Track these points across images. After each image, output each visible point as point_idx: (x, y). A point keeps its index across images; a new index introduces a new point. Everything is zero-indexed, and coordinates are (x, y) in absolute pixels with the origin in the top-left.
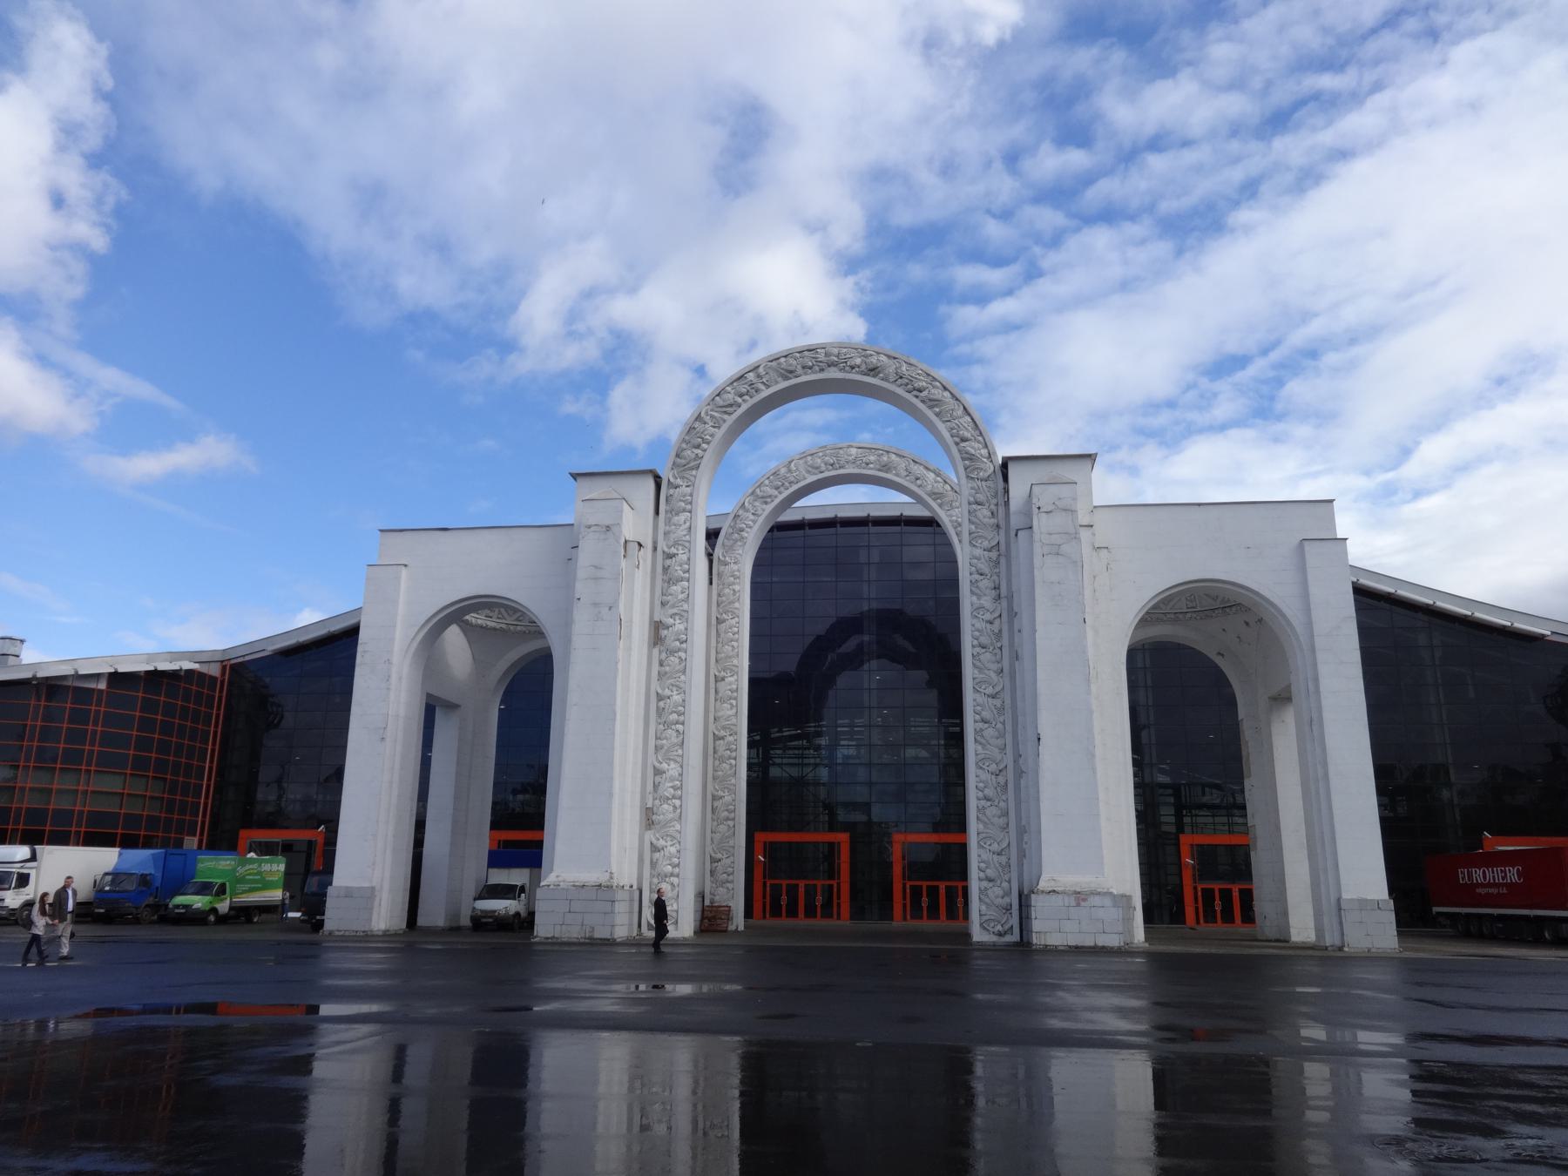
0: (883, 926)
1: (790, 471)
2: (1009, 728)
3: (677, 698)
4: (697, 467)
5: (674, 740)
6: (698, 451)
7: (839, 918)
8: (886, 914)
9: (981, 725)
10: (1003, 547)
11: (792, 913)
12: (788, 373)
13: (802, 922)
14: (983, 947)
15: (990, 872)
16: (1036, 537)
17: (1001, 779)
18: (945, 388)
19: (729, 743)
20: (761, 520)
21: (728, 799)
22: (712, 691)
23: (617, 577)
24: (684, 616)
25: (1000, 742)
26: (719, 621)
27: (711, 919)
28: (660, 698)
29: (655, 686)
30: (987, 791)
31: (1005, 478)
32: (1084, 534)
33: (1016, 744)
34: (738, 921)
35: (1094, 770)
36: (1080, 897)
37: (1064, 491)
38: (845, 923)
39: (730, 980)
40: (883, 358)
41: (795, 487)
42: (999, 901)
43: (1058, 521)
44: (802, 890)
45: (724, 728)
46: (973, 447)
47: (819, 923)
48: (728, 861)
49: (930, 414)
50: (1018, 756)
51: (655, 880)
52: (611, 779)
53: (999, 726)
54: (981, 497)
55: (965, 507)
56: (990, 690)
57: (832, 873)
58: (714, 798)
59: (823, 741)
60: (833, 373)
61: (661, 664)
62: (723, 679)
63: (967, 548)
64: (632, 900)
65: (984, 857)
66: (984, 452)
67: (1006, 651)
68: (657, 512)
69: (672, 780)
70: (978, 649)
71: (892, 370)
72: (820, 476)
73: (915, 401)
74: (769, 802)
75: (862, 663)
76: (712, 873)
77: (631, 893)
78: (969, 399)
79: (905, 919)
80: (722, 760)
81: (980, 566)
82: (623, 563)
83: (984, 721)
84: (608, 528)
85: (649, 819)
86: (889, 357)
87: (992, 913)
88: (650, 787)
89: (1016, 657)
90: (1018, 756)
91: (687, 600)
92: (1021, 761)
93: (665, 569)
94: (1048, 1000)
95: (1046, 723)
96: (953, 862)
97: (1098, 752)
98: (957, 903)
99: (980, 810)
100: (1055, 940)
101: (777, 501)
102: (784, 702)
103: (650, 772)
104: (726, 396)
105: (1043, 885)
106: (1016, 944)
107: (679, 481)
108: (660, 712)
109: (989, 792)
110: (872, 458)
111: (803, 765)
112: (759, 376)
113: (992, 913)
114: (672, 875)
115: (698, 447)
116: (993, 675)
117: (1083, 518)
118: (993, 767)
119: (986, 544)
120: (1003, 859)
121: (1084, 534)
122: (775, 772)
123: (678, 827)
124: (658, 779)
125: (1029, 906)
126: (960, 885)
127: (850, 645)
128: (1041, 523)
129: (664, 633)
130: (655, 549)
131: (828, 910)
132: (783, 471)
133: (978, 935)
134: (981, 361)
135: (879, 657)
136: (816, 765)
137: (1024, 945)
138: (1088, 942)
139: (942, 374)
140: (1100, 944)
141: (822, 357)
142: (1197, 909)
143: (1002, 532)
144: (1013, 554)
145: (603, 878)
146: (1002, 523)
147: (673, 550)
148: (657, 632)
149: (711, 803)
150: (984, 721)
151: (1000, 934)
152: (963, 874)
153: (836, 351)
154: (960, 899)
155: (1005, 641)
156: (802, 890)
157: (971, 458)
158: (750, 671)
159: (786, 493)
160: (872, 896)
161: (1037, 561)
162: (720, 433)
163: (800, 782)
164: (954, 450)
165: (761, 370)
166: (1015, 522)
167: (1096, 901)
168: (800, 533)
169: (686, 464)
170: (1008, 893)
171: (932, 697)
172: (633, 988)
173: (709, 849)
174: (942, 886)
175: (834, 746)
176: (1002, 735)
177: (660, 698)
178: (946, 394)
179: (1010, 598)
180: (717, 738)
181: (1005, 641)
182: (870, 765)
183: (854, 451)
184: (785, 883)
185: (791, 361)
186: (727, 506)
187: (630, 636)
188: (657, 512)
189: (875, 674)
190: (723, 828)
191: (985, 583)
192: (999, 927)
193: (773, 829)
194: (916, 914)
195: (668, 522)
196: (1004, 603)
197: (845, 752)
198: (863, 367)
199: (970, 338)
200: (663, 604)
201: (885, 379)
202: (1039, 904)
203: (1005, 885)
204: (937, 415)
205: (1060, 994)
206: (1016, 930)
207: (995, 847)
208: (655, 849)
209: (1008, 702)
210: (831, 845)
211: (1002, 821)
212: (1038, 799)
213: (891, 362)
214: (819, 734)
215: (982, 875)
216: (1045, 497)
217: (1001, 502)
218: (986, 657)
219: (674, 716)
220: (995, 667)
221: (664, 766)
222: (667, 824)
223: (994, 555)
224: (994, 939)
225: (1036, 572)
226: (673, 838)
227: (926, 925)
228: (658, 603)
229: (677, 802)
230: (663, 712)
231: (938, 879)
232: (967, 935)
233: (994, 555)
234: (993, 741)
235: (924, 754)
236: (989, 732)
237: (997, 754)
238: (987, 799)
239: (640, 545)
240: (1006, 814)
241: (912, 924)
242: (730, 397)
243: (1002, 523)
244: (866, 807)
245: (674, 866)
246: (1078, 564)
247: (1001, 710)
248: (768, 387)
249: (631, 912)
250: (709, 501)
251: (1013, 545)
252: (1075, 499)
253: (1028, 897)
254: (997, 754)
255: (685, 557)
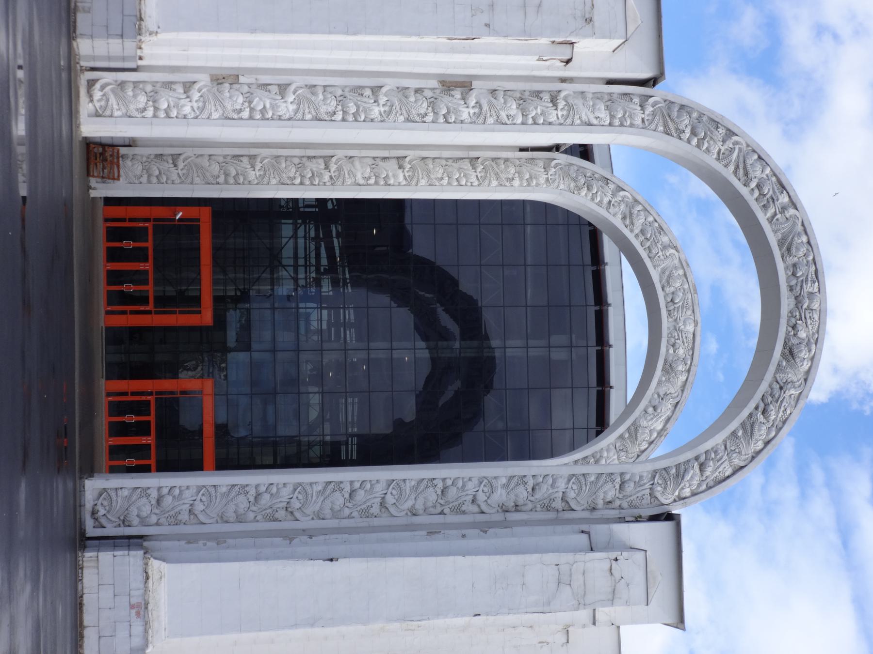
0: (100, 368)
1: (665, 248)
2: (346, 523)
3: (376, 111)
4: (667, 133)
5: (323, 109)
6: (687, 134)
7: (108, 313)
8: (116, 371)
9: (348, 489)
10: (569, 515)
11: (113, 255)
12: (787, 247)
13: (101, 266)
14: (77, 494)
15: (168, 501)
16: (580, 556)
17: (281, 514)
18: (767, 443)
19: (320, 175)
20: (602, 212)
21: (252, 175)
22: (385, 154)
23: (527, 33)
24: (479, 119)
25: (327, 512)
26: (474, 161)
27: (102, 155)
28: (376, 90)
29: (390, 84)
30: (267, 497)
31: (654, 518)
32: (584, 615)
33: (324, 532)
34: (101, 190)
35: (296, 626)
36: (142, 609)
37: (638, 590)
38: (101, 321)
39: (32, 183)
40: (806, 366)
41: (644, 254)
42: (134, 511)
43: (599, 582)
44: (142, 266)
45: (339, 169)
46: (693, 477)
47: (101, 288)
48: (174, 177)
49: (735, 424)
50: (310, 534)
51: (149, 88)
52: (273, 30)
53: (347, 512)
54: (630, 488)
55: (617, 470)
56: (390, 499)
57: (164, 303)
58: (252, 158)
59: (326, 288)
60: (786, 303)
61: (418, 91)
62: (401, 167)
63: (566, 472)
64: (124, 59)
65: (187, 494)
66: (687, 492)
67: (440, 519)
68: (610, 82)
69: (274, 107)
70: (440, 485)
71: (791, 376)
72: (658, 287)
73: (752, 405)
74: (249, 226)
75: (425, 338)
76: (160, 156)
77: (132, 58)
78: (753, 476)
79: (108, 394)
80: (300, 167)
81: (544, 488)
82: (544, 41)
83: (352, 493)
84: (589, 20)
85: (223, 79)
86: (808, 372)
87: (119, 503)
88: (265, 79)
89: (432, 532)
90: (310, 534)
91: (499, 122)
92: (304, 538)
93: (537, 94)
94: (21, 573)
95: (351, 569)
96: (176, 449)
97: (318, 631)
98: (130, 460)
99: (244, 489)
100: (89, 578)
101: (626, 232)
102: (372, 239)
103: (283, 79)
104: (758, 167)
105: (155, 565)
106: (83, 533)
107: (649, 109)
108: (358, 90)
109: (266, 499)
110: (681, 352)
111: (296, 267)
112: (783, 209)
113: (119, 503)
114: (156, 109)
115: (694, 133)
116: (409, 504)
117: (602, 614)
118: (296, 504)
119: (571, 494)
120: (184, 516)
121: (584, 615)
122: (287, 230)
123: (215, 115)
124: (275, 89)
125: (129, 547)
126: (152, 462)
127: (446, 320)
128: (598, 561)
129: (457, 93)
130: (563, 80)
131: (118, 299)
132: (665, 239)
133: (92, 486)
134: (804, 496)
135: (434, 360)
136: (296, 280)
137: (82, 541)
138: (88, 618)
139: (786, 444)
140: (87, 633)
141: (808, 288)
142: (125, 394)
143: (586, 514)
144: (559, 528)
145: (150, 23)
146: (597, 515)
147: (561, 104)
148: (458, 85)
149: (245, 154)
150: (352, 493)
151: (94, 513)
152: (167, 466)
153: (815, 306)
154: (134, 462)
155: (451, 518)
156: (142, 266)
157: (680, 473)
158: (411, 201)
159: (636, 244)
160: (137, 353)
161: (550, 558)
162: (711, 160)
163: (274, 261)
164: (690, 455)
165: (791, 212)
166: (600, 531)
167: (137, 629)
168: (588, 259)
169: (675, 118)
170: (144, 522)
171: (382, 426)
172: (20, 62)
173: (189, 152)
174: (149, 440)
175: (320, 299)
176: (335, 515)
177: (376, 90)
178: (760, 445)
179: (505, 524)
180: (327, 159)
181: (451, 518)
182: (298, 350)
183: (690, 328)
184: (150, 289)
185: (803, 250)
186: (621, 171)
187: (453, 50)
188: (610, 82)
189: (411, 355)
190: (215, 168)
191: (522, 493)
192: (102, 512)
193: (216, 229)
194: (117, 409)
195: (598, 96)
196: (499, 517)
197: (314, 316)
198: (794, 341)
199: (831, 483)
200: (493, 92)
201: (779, 367)
202: (133, 558)
203: (154, 519)
204: (734, 434)
205: (28, 588)
206: (99, 532)
207: (199, 507)
208: (188, 86)
209: (376, 522)
210: (196, 300)
211: (231, 515)
212: (257, 558)
213: (801, 376)
214: (335, 283)
215: (165, 491)
216: (630, 567)
217: (624, 513)
218: (432, 496)
219: (353, 110)
220: (419, 506)
221: (291, 98)
222: (220, 102)
223: (558, 504)
224: (89, 506)
225: (535, 557)
226: (202, 109)
227: (102, 421)
228: (494, 85)
229: (246, 114)
230: (357, 93)
231: (159, 436)
232: (90, 471)
233: (558, 504)
234: (328, 503)
235: (314, 414)
236: (339, 500)
237: (311, 509)
238: (258, 496)
239: (568, 62)
240: (240, 519)
241: (102, 404)
242: (757, 172)
243: (597, 515)
244: (245, 345)
245: (167, 112)
246: (546, 607)
247: (366, 513)
248: (770, 220)
249: (109, 58)
250: (626, 145)
251: (568, 528)
252: (627, 603)
253: (140, 547)
254: (311, 509)
255: (553, 118)
